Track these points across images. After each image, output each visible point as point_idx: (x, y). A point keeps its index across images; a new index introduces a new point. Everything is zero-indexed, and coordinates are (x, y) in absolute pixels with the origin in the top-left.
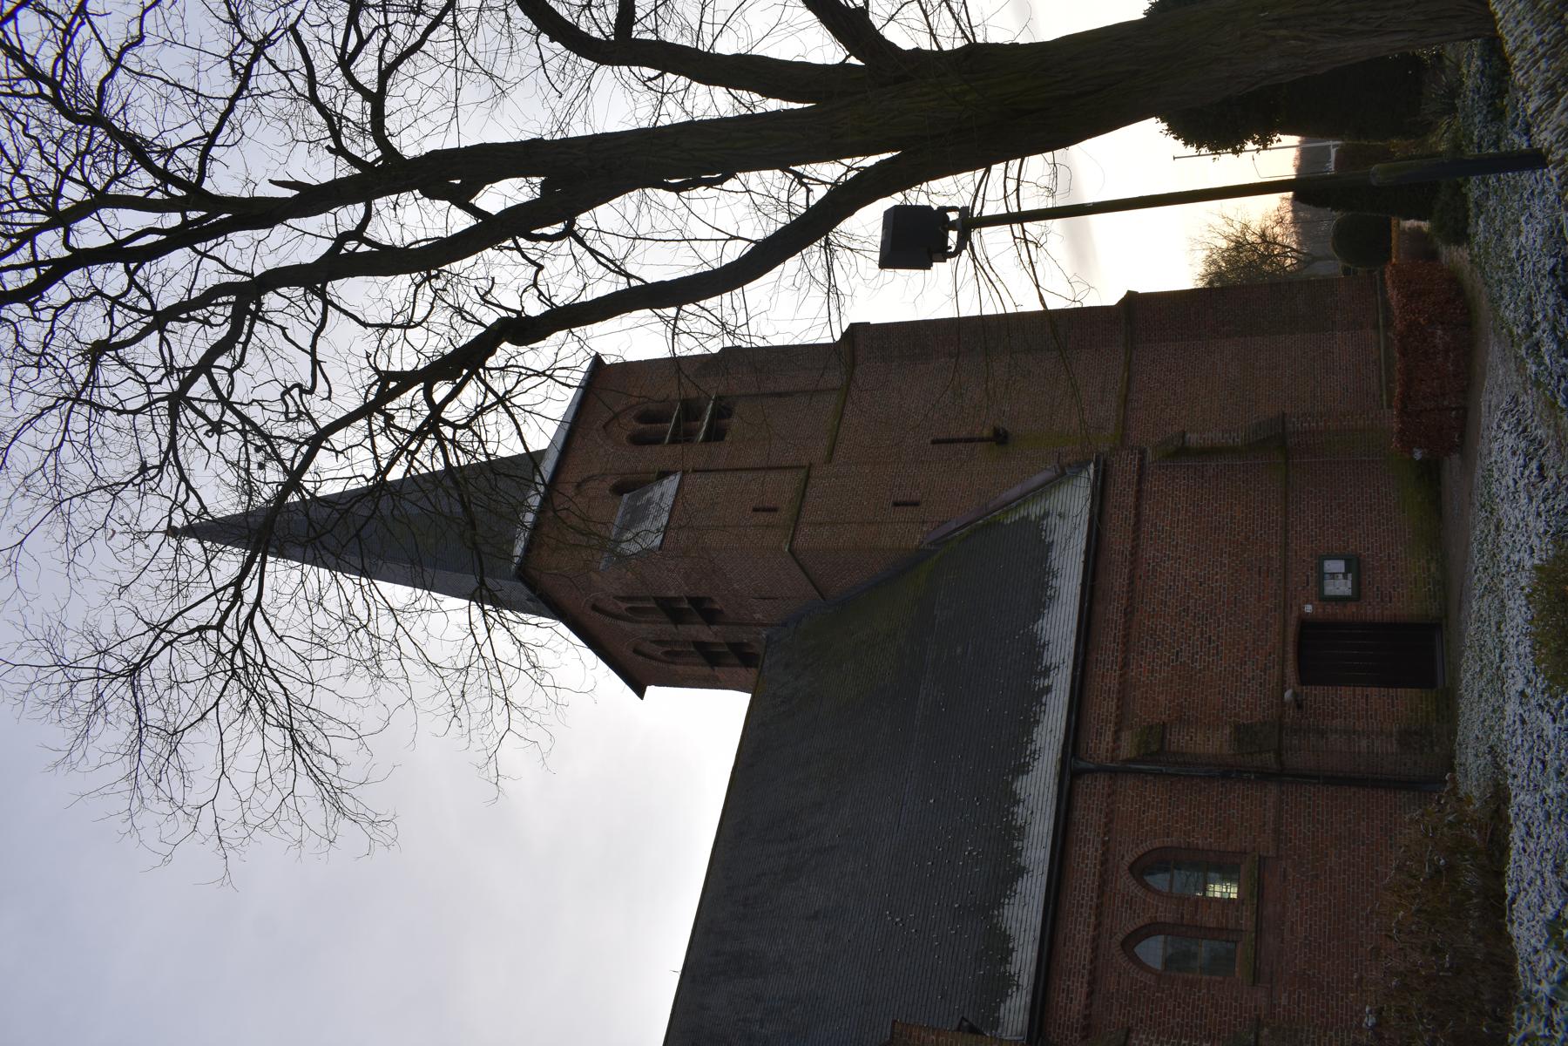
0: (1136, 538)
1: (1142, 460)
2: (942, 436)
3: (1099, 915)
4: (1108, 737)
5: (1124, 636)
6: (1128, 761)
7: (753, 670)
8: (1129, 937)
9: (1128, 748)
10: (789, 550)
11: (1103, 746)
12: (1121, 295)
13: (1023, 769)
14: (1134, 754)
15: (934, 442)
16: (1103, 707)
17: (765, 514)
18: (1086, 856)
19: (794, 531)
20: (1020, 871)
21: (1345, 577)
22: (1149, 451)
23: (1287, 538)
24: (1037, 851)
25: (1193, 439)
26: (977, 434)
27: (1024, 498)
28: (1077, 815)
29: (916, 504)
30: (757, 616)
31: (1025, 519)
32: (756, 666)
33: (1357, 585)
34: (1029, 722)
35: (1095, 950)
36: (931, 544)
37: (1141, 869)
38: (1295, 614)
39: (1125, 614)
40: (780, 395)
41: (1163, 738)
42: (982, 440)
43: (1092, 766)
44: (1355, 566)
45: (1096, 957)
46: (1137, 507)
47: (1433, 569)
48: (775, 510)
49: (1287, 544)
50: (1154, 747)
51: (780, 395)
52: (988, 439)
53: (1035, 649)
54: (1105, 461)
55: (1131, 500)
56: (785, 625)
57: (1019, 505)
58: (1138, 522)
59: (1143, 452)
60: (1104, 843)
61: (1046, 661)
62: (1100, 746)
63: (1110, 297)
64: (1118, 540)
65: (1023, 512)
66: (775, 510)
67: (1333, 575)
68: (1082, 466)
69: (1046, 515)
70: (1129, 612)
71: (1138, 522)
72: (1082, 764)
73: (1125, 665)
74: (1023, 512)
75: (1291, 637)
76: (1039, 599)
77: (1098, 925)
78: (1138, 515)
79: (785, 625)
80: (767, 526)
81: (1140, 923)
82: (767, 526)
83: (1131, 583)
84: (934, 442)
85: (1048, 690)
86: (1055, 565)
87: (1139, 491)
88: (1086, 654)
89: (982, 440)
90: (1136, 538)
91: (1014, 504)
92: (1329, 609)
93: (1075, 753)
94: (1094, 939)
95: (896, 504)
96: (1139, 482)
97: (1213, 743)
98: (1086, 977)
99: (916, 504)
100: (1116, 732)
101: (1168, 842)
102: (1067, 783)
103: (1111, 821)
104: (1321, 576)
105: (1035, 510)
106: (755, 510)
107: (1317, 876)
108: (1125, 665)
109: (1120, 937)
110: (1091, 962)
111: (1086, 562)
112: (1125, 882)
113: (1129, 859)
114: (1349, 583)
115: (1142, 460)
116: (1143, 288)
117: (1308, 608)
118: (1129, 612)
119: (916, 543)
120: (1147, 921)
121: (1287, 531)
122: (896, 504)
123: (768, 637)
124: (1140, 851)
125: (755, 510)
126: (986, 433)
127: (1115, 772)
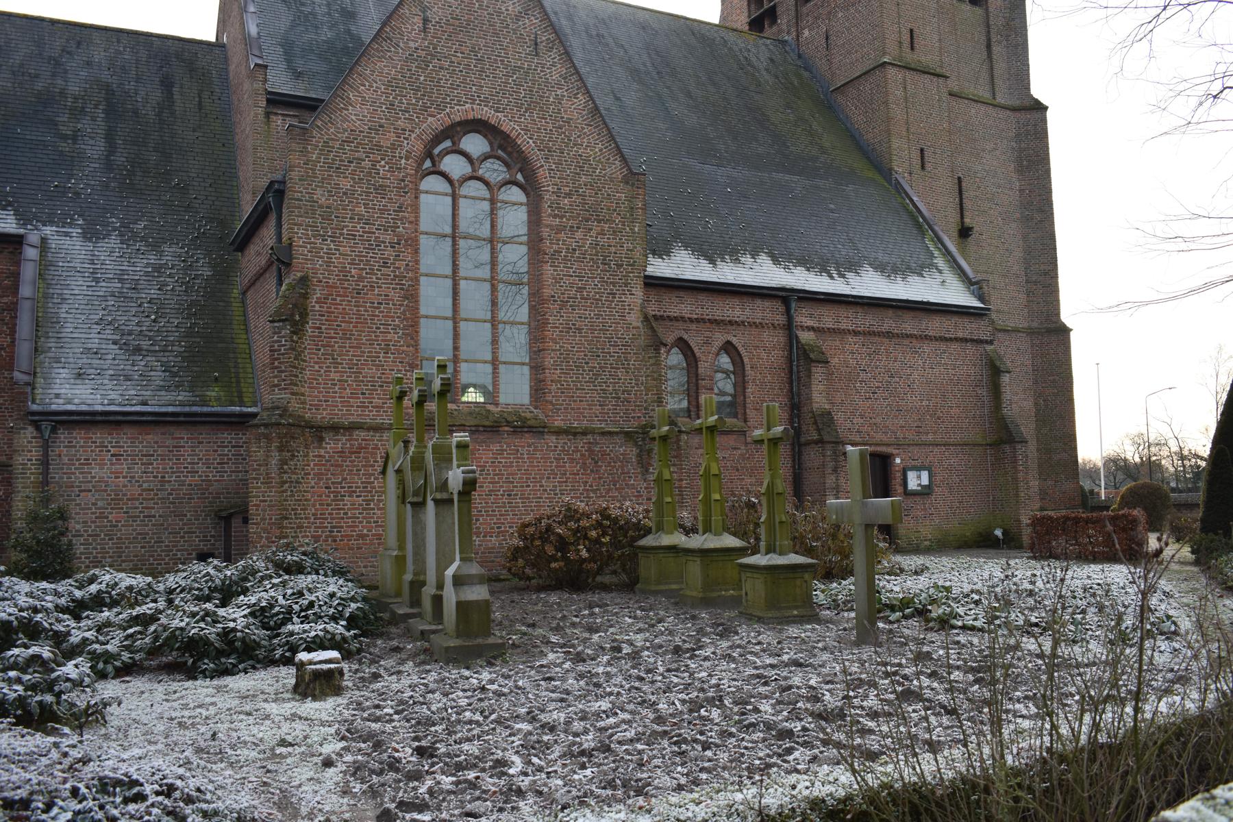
0: (936, 339)
1: (987, 342)
2: (964, 184)
3: (698, 320)
4: (810, 323)
5: (874, 332)
6: (798, 342)
7: (747, 28)
8: (686, 342)
9: (806, 337)
10: (885, 62)
11: (804, 319)
12: (1069, 325)
13: (776, 260)
14: (803, 342)
15: (959, 178)
16: (828, 317)
17: (909, 40)
18: (734, 310)
19: (899, 66)
20: (712, 262)
21: (919, 485)
22: (992, 347)
23: (940, 445)
24: (727, 273)
25: (1006, 379)
26: (966, 213)
27: (947, 253)
28: (759, 302)
29: (923, 167)
30: (806, 33)
31: (932, 256)
32: (750, 30)
33: (914, 494)
34: (806, 262)
35: (676, 319)
36: (896, 179)
37: (728, 348)
38: (895, 452)
39: (888, 333)
40: (989, 47)
41: (819, 362)
42: (962, 217)
43: (792, 311)
44: (926, 492)
45: (671, 320)
46: (956, 339)
47: (926, 543)
48: (912, 48)
49: (937, 445)
50: (812, 356)
51: (989, 47)
52: (963, 223)
53: (850, 266)
54: (985, 315)
55: (960, 335)
56: (800, 56)
57: (940, 250)
58: (946, 340)
59: (991, 342)
60: (743, 322)
61: (849, 275)
62: (804, 317)
63: (1066, 317)
64: (935, 325)
65: (936, 253)
66: (912, 48)
67: (919, 477)
68: (981, 298)
69: (940, 272)
70: (889, 335)
71: (946, 340)
72: (793, 305)
73: (856, 333)
74: (936, 253)
75: (879, 449)
76: (888, 270)
77: (691, 320)
78: (951, 339)
79: (800, 56)
80: (900, 42)
81: (696, 350)
82: (900, 42)
83: (908, 336)
84: (959, 178)
85: (832, 277)
86: (910, 279)
87: (965, 340)
88: (863, 305)
89: (962, 217)
90: (936, 339)
91: (940, 246)
92: (898, 474)
93: (800, 299)
94: (682, 318)
95: (922, 150)
96: (972, 340)
97: (819, 397)
98: (658, 313)
99: (923, 167)
100: (813, 328)
101: (748, 367)
102: (781, 294)
103: (757, 326)
104: (918, 469)
105: (940, 262)
106: (911, 31)
107: (738, 470)
108: (856, 333)
109: (686, 337)
110: (668, 317)
111: (922, 303)
112: (720, 338)
113: (734, 340)
114: (915, 488)
115: (987, 342)
116: (1073, 336)
117: (898, 461)
118: (889, 335)
119: (896, 168)
120: (697, 355)
121: (944, 445)
122: (922, 150)
123: (786, 41)
124: (740, 349)
125: (911, 31)
126: (967, 221)
127: (789, 327)
